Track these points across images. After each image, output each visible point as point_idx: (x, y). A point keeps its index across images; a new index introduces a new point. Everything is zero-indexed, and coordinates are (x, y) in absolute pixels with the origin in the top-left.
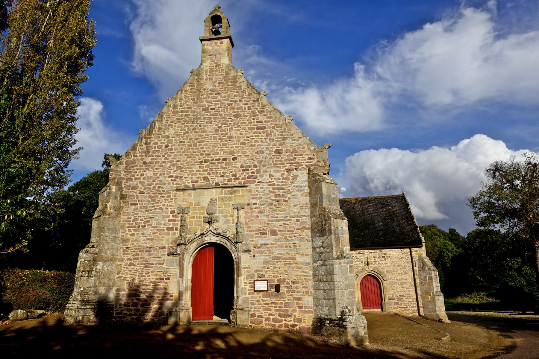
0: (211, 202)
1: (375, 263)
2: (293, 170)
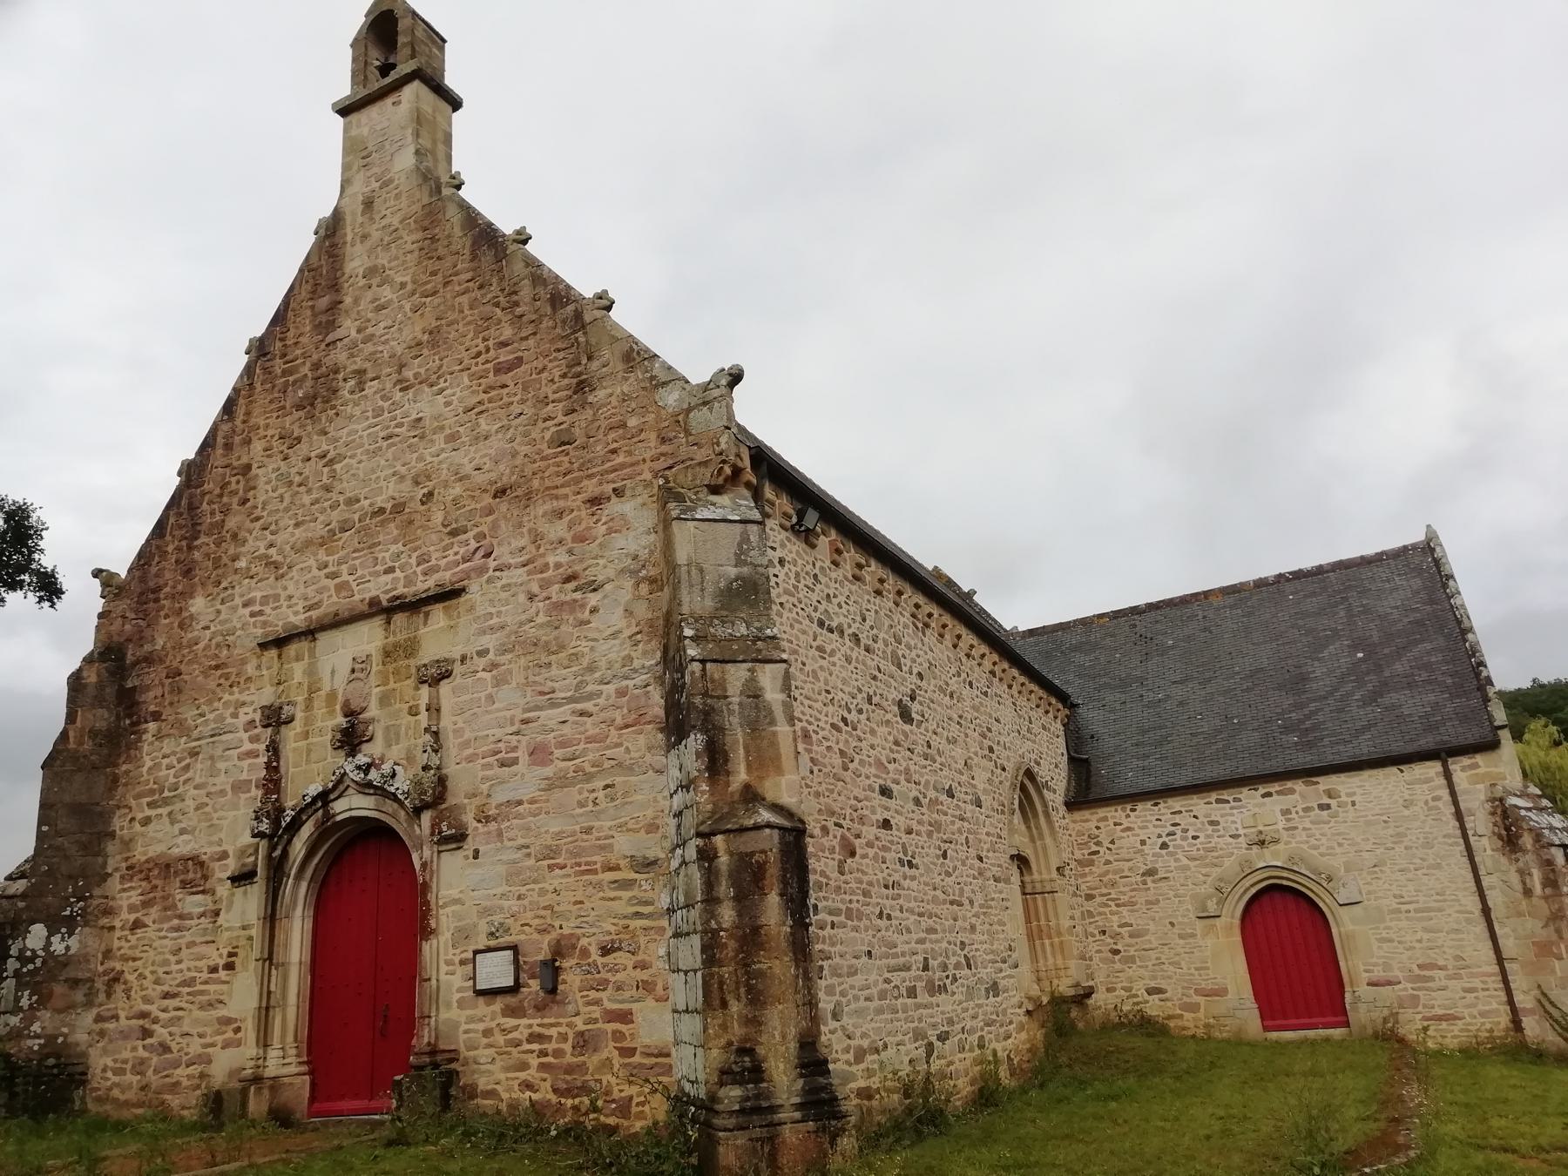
0: (353, 671)
1: (1293, 836)
2: (609, 499)
